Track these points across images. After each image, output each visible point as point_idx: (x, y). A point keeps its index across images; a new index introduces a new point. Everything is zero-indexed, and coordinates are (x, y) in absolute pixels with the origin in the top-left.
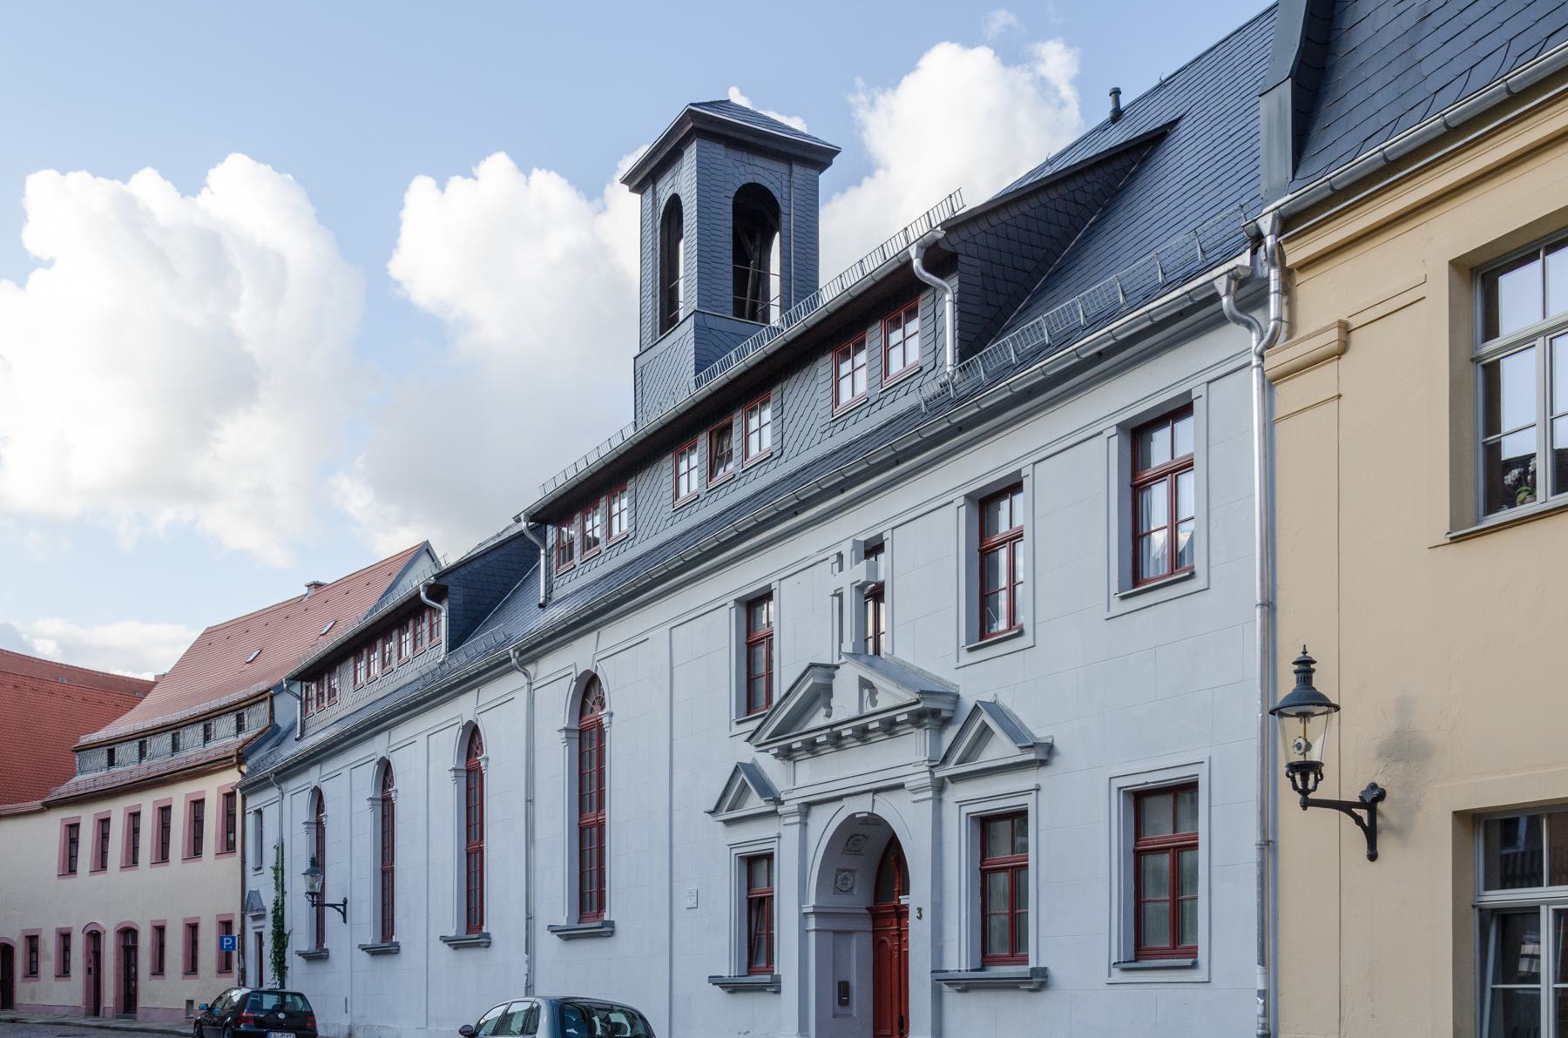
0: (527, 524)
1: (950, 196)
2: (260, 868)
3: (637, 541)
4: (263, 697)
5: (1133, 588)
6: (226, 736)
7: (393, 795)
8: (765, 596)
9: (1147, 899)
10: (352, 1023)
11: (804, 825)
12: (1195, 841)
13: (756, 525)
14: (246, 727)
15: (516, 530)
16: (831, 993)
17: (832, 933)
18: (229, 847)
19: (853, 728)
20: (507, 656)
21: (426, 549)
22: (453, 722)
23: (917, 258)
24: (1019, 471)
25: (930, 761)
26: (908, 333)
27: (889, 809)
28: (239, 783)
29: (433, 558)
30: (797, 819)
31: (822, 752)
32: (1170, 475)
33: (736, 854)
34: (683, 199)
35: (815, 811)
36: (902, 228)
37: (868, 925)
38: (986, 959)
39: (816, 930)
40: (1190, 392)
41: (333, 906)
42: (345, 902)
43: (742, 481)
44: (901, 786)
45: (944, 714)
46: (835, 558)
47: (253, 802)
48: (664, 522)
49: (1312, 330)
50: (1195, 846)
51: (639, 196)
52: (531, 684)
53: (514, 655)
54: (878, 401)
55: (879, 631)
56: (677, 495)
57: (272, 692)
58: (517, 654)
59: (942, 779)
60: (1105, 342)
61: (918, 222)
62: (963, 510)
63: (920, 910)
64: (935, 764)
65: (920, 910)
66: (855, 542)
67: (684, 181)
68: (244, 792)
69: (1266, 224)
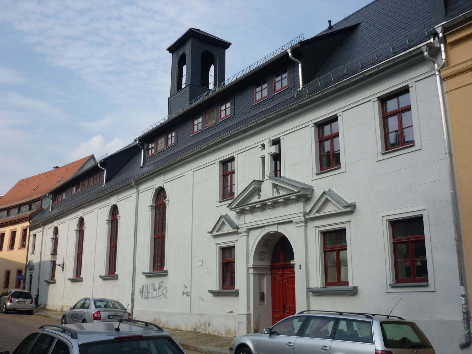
0: (139, 142)
1: (236, 75)
2: (33, 253)
3: (178, 146)
4: (39, 199)
6: (25, 211)
7: (84, 229)
8: (232, 159)
9: (341, 265)
10: (63, 305)
12: (424, 238)
13: (230, 136)
14: (32, 208)
15: (135, 144)
18: (23, 246)
20: (131, 182)
21: (92, 157)
22: (52, 227)
23: (290, 53)
25: (303, 212)
26: (263, 88)
27: (284, 230)
28: (29, 226)
29: (94, 159)
30: (303, 224)
33: (219, 247)
34: (186, 54)
35: (252, 232)
36: (281, 46)
38: (327, 283)
40: (337, 114)
41: (60, 265)
42: (64, 264)
43: (204, 133)
44: (291, 222)
45: (309, 196)
47: (33, 232)
48: (188, 140)
49: (67, 220)
50: (346, 249)
51: (172, 54)
52: (138, 191)
53: (133, 182)
54: (272, 98)
55: (277, 169)
56: (72, 194)
57: (42, 198)
58: (134, 182)
59: (308, 219)
62: (219, 165)
63: (300, 266)
64: (305, 214)
65: (300, 266)
66: (270, 140)
67: (188, 49)
68: (30, 229)
69: (439, 30)
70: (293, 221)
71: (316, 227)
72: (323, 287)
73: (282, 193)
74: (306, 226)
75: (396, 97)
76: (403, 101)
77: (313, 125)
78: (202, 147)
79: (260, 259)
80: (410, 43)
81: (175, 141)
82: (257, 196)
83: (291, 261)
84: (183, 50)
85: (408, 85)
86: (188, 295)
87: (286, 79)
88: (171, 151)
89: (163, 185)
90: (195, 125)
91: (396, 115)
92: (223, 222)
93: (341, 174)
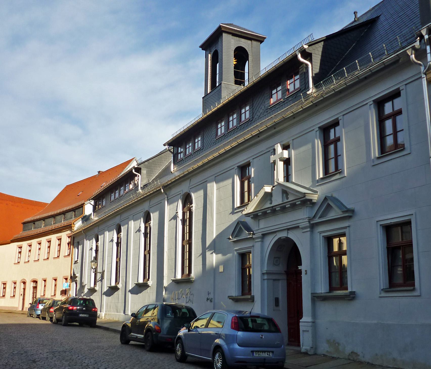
3: (204, 150)
5: (381, 155)
11: (262, 241)
16: (273, 303)
17: (272, 280)
19: (301, 201)
24: (338, 118)
26: (278, 90)
27: (293, 236)
30: (309, 229)
32: (334, 142)
37: (285, 277)
38: (331, 289)
44: (298, 227)
46: (272, 151)
48: (212, 144)
59: (313, 224)
60: (363, 76)
61: (307, 38)
62: (318, 132)
64: (310, 220)
69: (424, 32)
70: (300, 227)
72: (327, 292)
73: (291, 198)
74: (262, 241)
75: (391, 101)
76: (398, 103)
77: (317, 129)
78: (336, 89)
79: (274, 264)
80: (388, 52)
81: (201, 146)
83: (298, 267)
84: (216, 47)
85: (399, 88)
86: (211, 301)
87: (298, 80)
88: (296, 98)
89: (189, 191)
90: (243, 113)
91: (391, 118)
92: (240, 228)
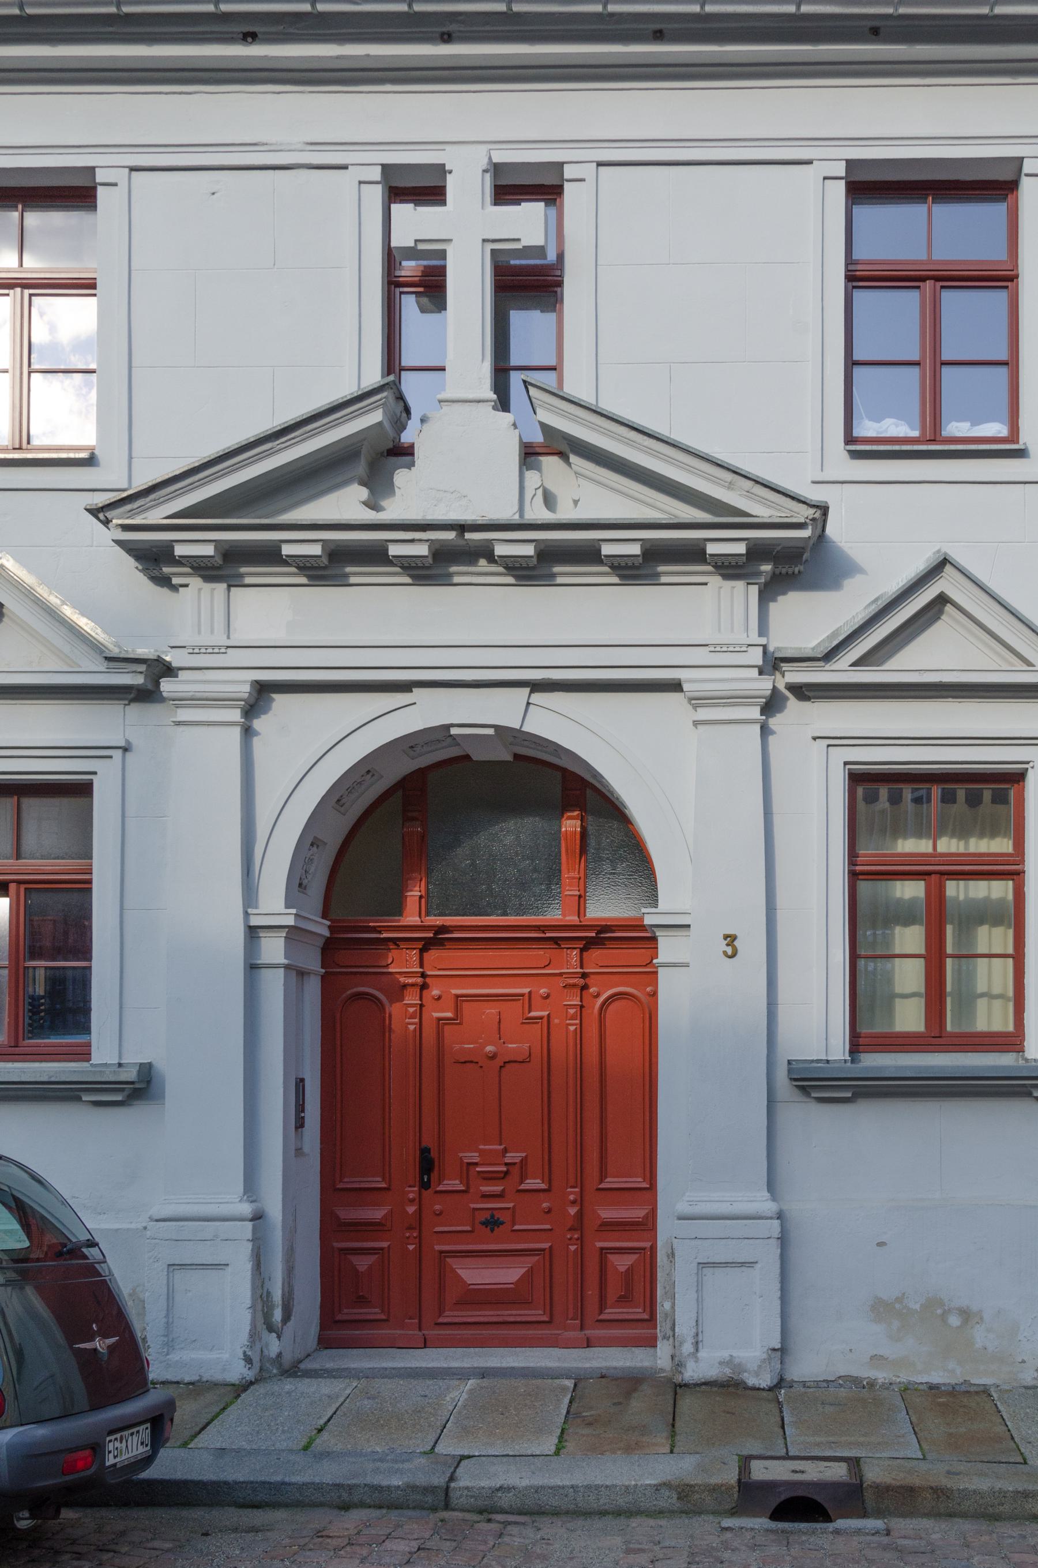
31: (248, 580)
39: (287, 967)
44: (675, 686)
63: (731, 939)
71: (834, 741)
82: (358, 492)
93: (92, 492)
